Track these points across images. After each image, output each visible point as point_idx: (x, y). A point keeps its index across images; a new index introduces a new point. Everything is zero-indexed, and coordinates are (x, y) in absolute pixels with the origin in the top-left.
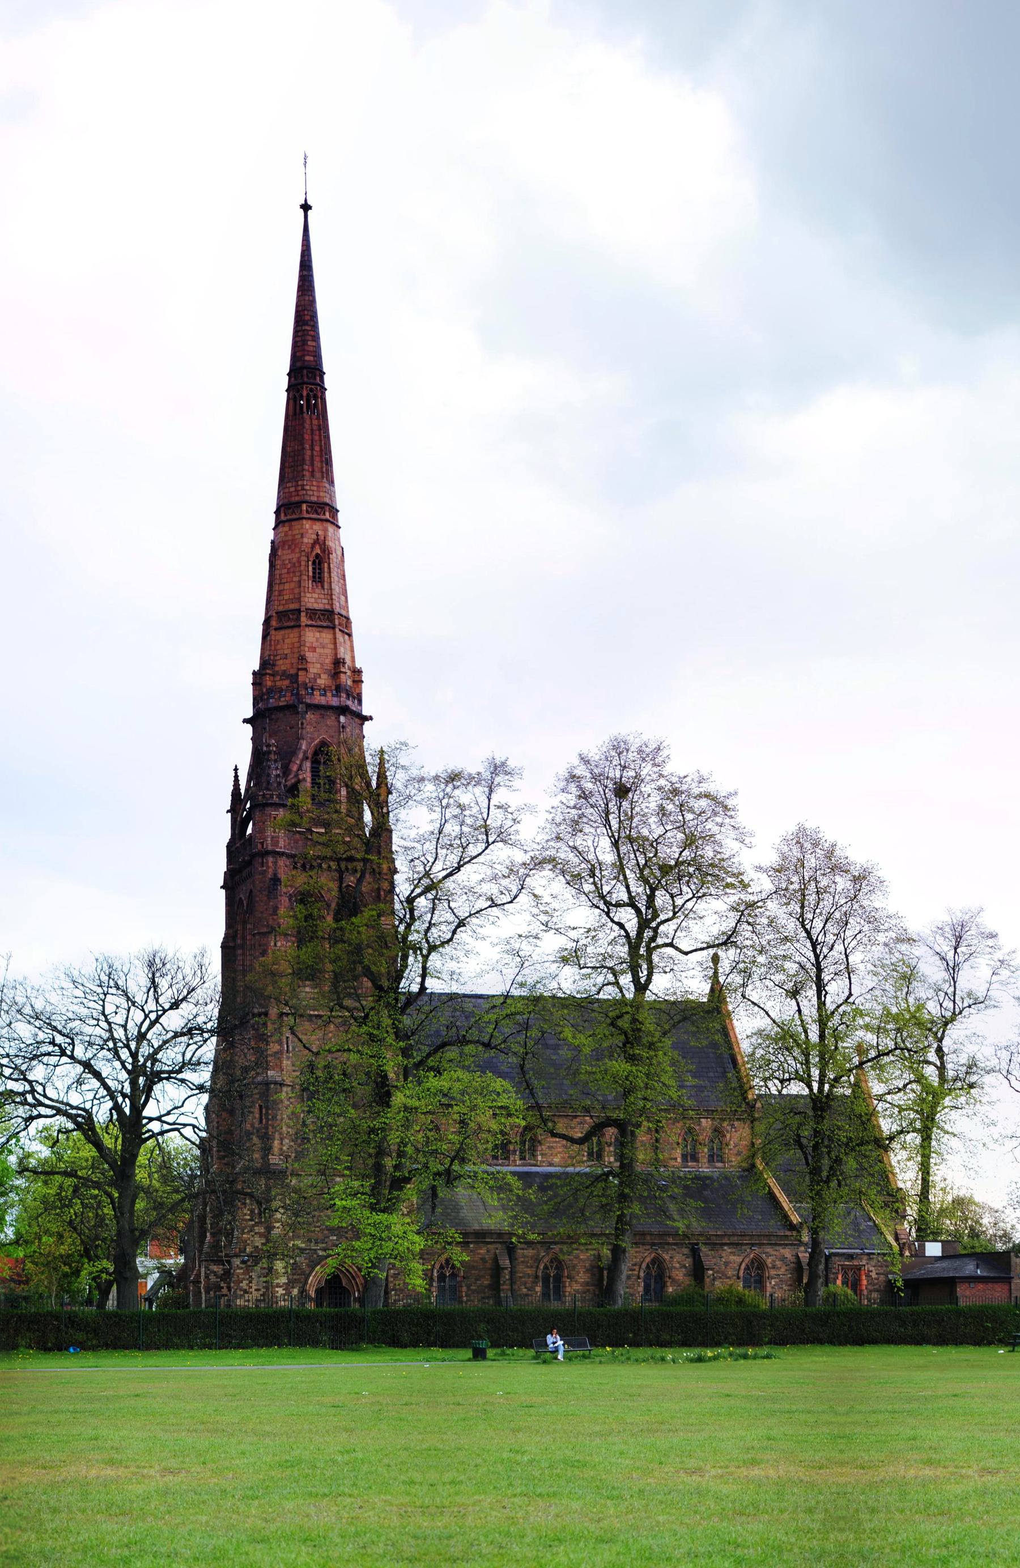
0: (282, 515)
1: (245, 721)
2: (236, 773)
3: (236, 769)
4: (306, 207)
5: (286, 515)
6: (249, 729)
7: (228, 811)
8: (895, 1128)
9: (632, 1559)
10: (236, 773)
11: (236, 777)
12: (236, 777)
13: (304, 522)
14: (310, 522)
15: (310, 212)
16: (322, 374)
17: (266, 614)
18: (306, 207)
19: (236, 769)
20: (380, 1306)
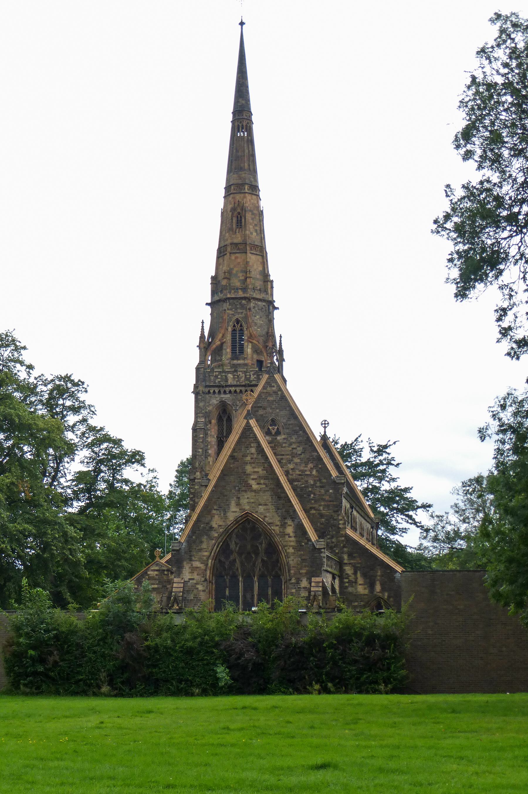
0: (237, 115)
1: (207, 304)
2: (203, 325)
3: (203, 322)
4: (242, 24)
5: (239, 116)
6: (209, 309)
7: (198, 346)
8: (518, 208)
9: (474, 518)
10: (203, 325)
11: (203, 327)
12: (203, 327)
13: (247, 195)
14: (250, 195)
15: (244, 26)
16: (270, 306)
17: (219, 245)
18: (242, 24)
19: (203, 322)
20: (325, 568)
